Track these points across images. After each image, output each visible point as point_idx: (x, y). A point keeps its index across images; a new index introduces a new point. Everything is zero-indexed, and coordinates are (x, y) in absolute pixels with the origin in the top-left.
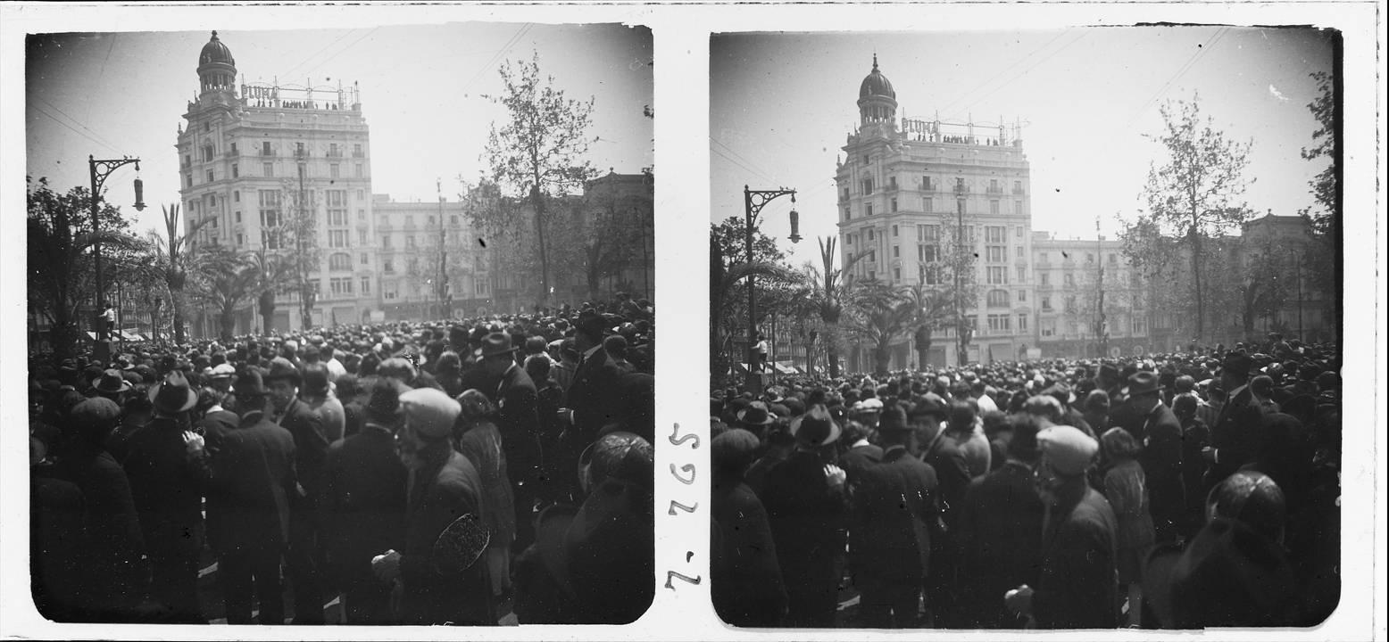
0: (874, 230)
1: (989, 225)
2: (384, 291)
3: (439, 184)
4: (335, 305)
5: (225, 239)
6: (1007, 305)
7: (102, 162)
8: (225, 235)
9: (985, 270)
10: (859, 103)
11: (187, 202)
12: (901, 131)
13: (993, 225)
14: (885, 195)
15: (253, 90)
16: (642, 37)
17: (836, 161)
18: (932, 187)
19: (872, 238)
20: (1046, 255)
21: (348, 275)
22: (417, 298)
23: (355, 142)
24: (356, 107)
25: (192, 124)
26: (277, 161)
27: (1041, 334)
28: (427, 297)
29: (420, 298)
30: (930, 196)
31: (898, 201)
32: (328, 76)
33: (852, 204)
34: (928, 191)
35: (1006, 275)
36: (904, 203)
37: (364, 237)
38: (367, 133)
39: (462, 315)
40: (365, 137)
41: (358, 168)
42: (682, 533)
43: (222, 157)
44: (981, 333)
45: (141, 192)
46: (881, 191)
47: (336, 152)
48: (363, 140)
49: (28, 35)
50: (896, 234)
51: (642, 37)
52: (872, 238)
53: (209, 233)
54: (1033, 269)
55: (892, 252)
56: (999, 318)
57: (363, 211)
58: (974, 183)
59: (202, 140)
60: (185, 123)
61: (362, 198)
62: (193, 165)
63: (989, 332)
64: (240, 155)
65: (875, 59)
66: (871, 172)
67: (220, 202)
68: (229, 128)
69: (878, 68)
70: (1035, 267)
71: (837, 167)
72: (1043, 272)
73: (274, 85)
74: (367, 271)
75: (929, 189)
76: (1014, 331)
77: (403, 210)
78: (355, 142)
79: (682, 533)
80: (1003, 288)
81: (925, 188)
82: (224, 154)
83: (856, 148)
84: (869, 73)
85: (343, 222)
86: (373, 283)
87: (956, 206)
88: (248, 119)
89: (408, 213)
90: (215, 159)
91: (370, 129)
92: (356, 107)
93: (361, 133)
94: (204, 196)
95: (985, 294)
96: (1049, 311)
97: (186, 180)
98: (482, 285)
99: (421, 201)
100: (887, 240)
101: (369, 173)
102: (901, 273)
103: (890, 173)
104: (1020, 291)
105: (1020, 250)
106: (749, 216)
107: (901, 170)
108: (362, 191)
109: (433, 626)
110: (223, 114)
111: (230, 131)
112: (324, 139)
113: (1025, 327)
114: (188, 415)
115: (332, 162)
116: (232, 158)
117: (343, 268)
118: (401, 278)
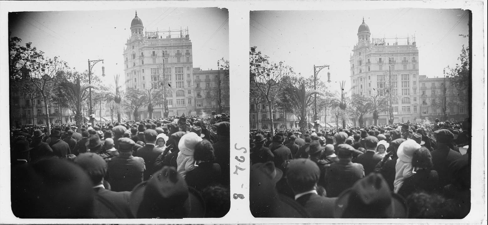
0: (136, 71)
1: (152, 68)
2: (422, 111)
3: (444, 71)
4: (403, 116)
5: (365, 93)
6: (409, 103)
7: (92, 61)
8: (365, 91)
9: (401, 90)
10: (358, 34)
11: (353, 80)
12: (372, 43)
13: (154, 68)
14: (140, 59)
15: (376, 40)
16: (225, 12)
17: (123, 49)
18: (382, 62)
19: (361, 81)
20: (198, 76)
21: (409, 105)
22: (210, 107)
23: (186, 49)
24: (414, 43)
25: (355, 53)
26: (157, 58)
27: (197, 106)
28: (214, 106)
29: (436, 114)
30: (394, 65)
31: (370, 67)
32: (115, 27)
33: (355, 69)
34: (154, 56)
35: (397, 92)
36: (146, 61)
37: (415, 91)
38: (418, 53)
39: (454, 120)
40: (190, 47)
41: (414, 66)
42: (240, 181)
43: (365, 64)
44: (174, 106)
45: (330, 76)
46: (138, 57)
47: (394, 61)
48: (416, 55)
49: (9, 12)
50: (143, 72)
51: (225, 12)
52: (361, 81)
53: (360, 91)
54: (193, 82)
55: (142, 78)
56: (406, 108)
57: (415, 82)
58: (397, 59)
59: (132, 52)
60: (353, 53)
61: (189, 70)
62: (355, 67)
63: (177, 105)
64: (371, 63)
65: (136, 12)
66: (361, 58)
67: (137, 73)
68: (140, 47)
69: (137, 16)
70: (420, 88)
71: (350, 57)
72: (198, 83)
73: (157, 31)
74: (416, 104)
75: (381, 62)
76: (412, 112)
77: (431, 81)
78: (186, 49)
79: (240, 181)
80: (182, 89)
81: (153, 56)
82: (139, 57)
83: (357, 50)
84: (134, 17)
85: (407, 86)
86: (418, 108)
87: (100, 61)
88: (374, 50)
89: (207, 75)
90: (136, 58)
91: (419, 52)
92: (414, 43)
93: (416, 53)
94: (132, 71)
95: (401, 99)
96: (426, 105)
97: (352, 72)
98: (462, 109)
99: (438, 77)
100: (140, 75)
101: (192, 60)
102: (145, 85)
103: (141, 51)
104: (414, 97)
105: (415, 83)
106: (315, 75)
107: (145, 50)
108: (415, 74)
109: (153, 219)
110: (365, 49)
111: (141, 48)
112: (401, 56)
113: (416, 111)
114: (292, 157)
115: (153, 58)
116: (142, 58)
117: (181, 95)
118: (203, 99)
